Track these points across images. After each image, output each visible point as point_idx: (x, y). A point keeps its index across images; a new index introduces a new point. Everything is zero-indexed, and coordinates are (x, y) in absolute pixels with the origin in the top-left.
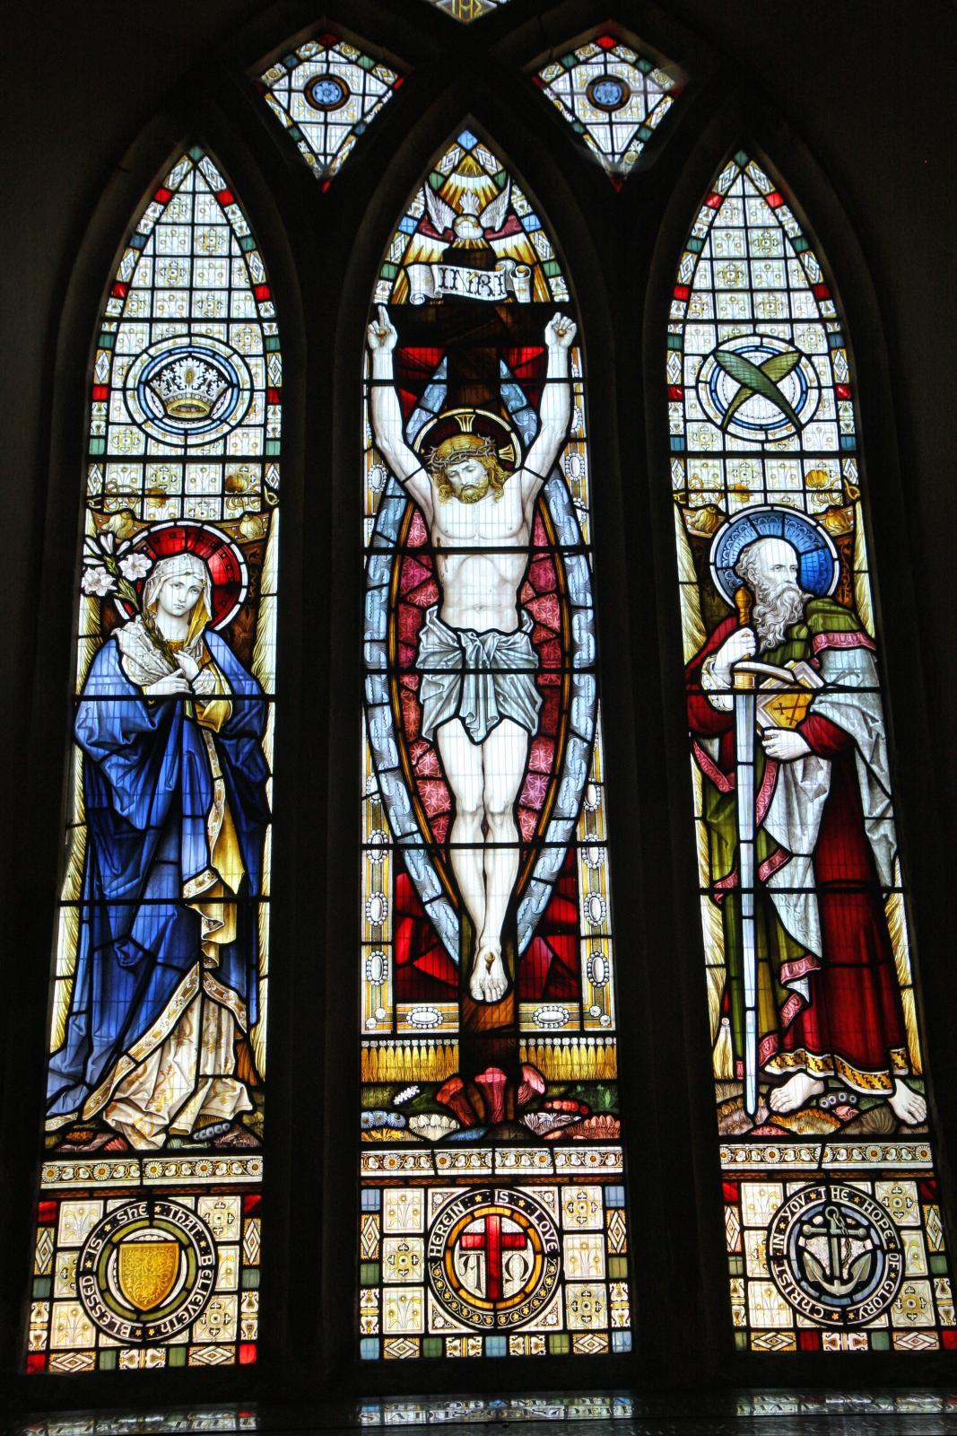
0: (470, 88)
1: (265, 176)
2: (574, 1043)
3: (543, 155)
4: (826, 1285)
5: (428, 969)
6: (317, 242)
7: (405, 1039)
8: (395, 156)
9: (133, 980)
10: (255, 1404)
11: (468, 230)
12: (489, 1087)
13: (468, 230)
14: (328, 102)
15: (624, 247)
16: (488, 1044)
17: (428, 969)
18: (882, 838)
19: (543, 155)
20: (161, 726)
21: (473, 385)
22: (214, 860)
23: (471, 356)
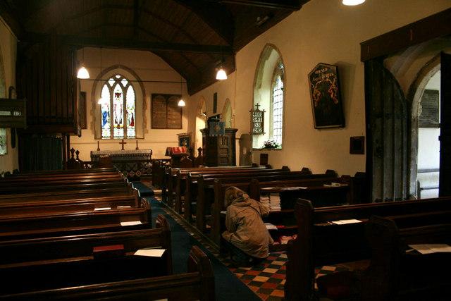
0: (118, 81)
1: (109, 85)
2: (122, 125)
3: (121, 85)
4: (114, 95)
5: (116, 123)
6: (111, 89)
7: (115, 125)
8: (115, 85)
9: (105, 122)
10: (220, 62)
11: (118, 89)
12: (118, 127)
13: (118, 89)
14: (112, 82)
15: (125, 90)
16: (118, 125)
17: (116, 123)
18: (8, 296)
19: (121, 85)
20: (105, 112)
21: (118, 97)
22: (108, 118)
23: (118, 95)
